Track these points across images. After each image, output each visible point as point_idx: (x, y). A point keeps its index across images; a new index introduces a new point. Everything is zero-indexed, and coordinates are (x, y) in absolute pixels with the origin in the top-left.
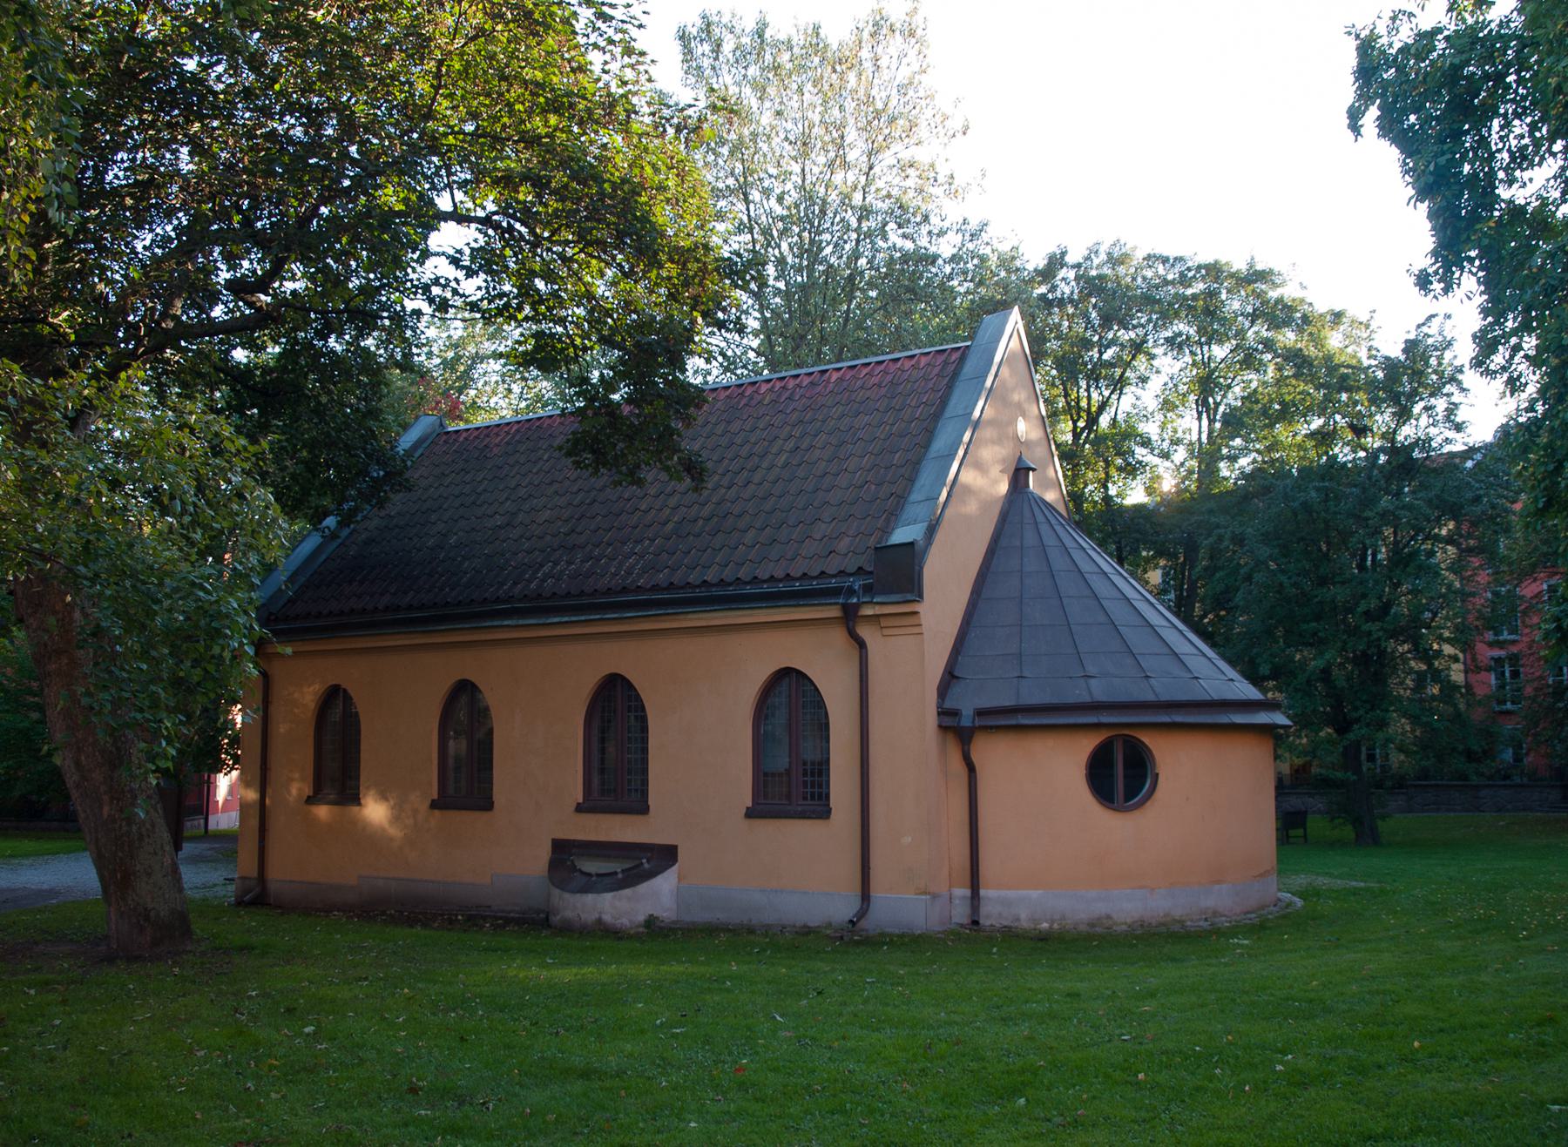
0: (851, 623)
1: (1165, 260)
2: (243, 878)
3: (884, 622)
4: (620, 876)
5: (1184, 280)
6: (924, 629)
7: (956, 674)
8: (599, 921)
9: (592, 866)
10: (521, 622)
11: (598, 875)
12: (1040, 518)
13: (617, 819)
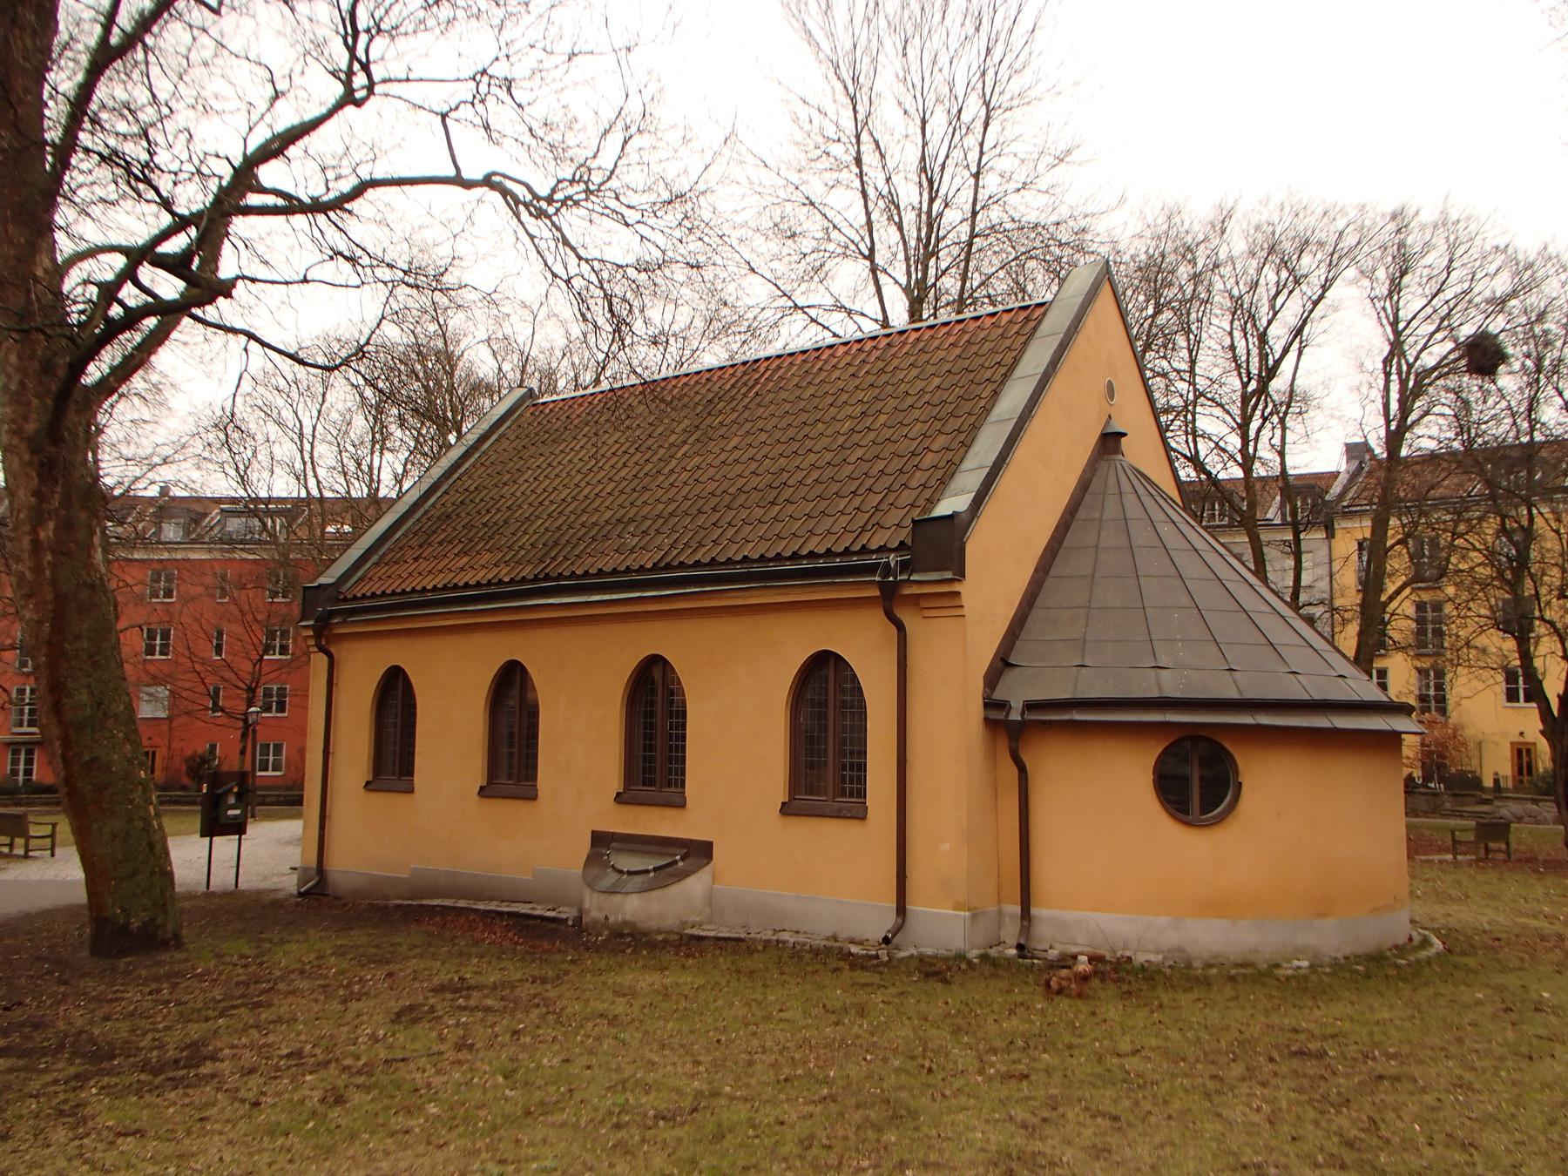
3: (924, 604)
6: (966, 611)
7: (1011, 661)
9: (628, 862)
11: (630, 873)
12: (1126, 486)
13: (655, 813)
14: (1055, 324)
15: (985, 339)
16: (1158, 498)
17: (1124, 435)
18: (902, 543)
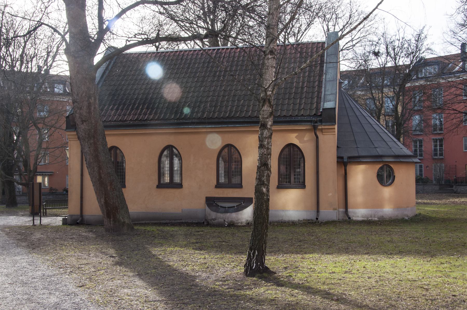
4: (236, 207)
10: (196, 127)
11: (228, 207)
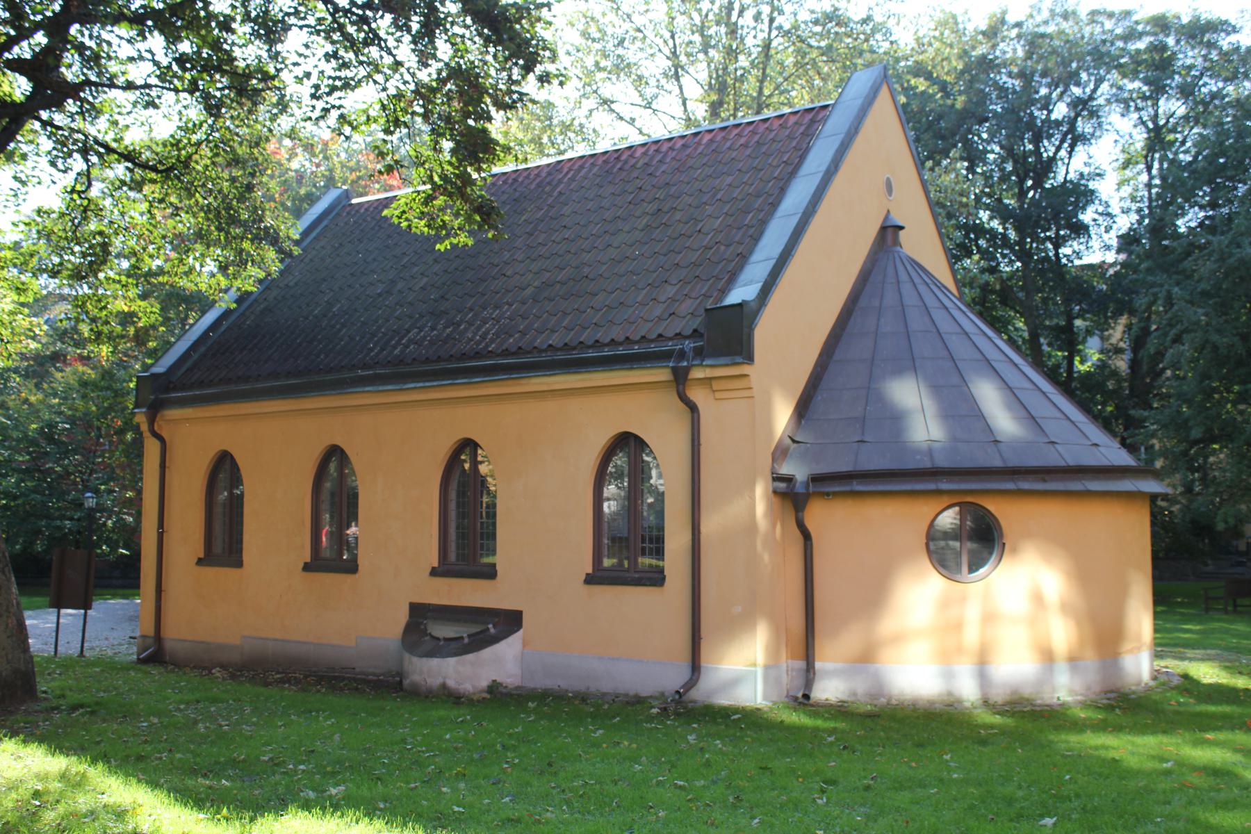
0: (681, 387)
1: (1111, 15)
2: (144, 637)
3: (716, 385)
4: (466, 640)
5: (1131, 35)
8: (444, 686)
9: (443, 631)
10: (381, 388)
11: (446, 640)
12: (903, 276)
14: (835, 126)
15: (773, 140)
16: (933, 287)
17: (902, 228)
18: (695, 331)
